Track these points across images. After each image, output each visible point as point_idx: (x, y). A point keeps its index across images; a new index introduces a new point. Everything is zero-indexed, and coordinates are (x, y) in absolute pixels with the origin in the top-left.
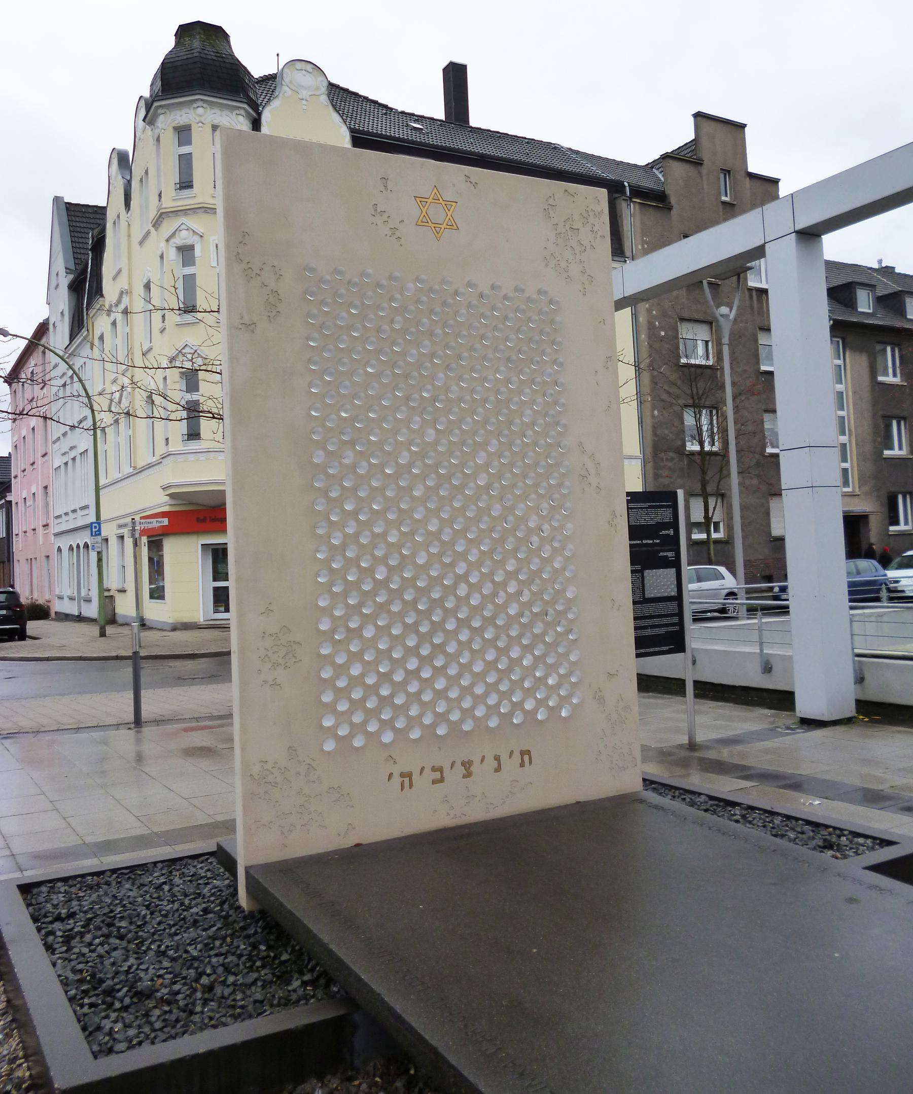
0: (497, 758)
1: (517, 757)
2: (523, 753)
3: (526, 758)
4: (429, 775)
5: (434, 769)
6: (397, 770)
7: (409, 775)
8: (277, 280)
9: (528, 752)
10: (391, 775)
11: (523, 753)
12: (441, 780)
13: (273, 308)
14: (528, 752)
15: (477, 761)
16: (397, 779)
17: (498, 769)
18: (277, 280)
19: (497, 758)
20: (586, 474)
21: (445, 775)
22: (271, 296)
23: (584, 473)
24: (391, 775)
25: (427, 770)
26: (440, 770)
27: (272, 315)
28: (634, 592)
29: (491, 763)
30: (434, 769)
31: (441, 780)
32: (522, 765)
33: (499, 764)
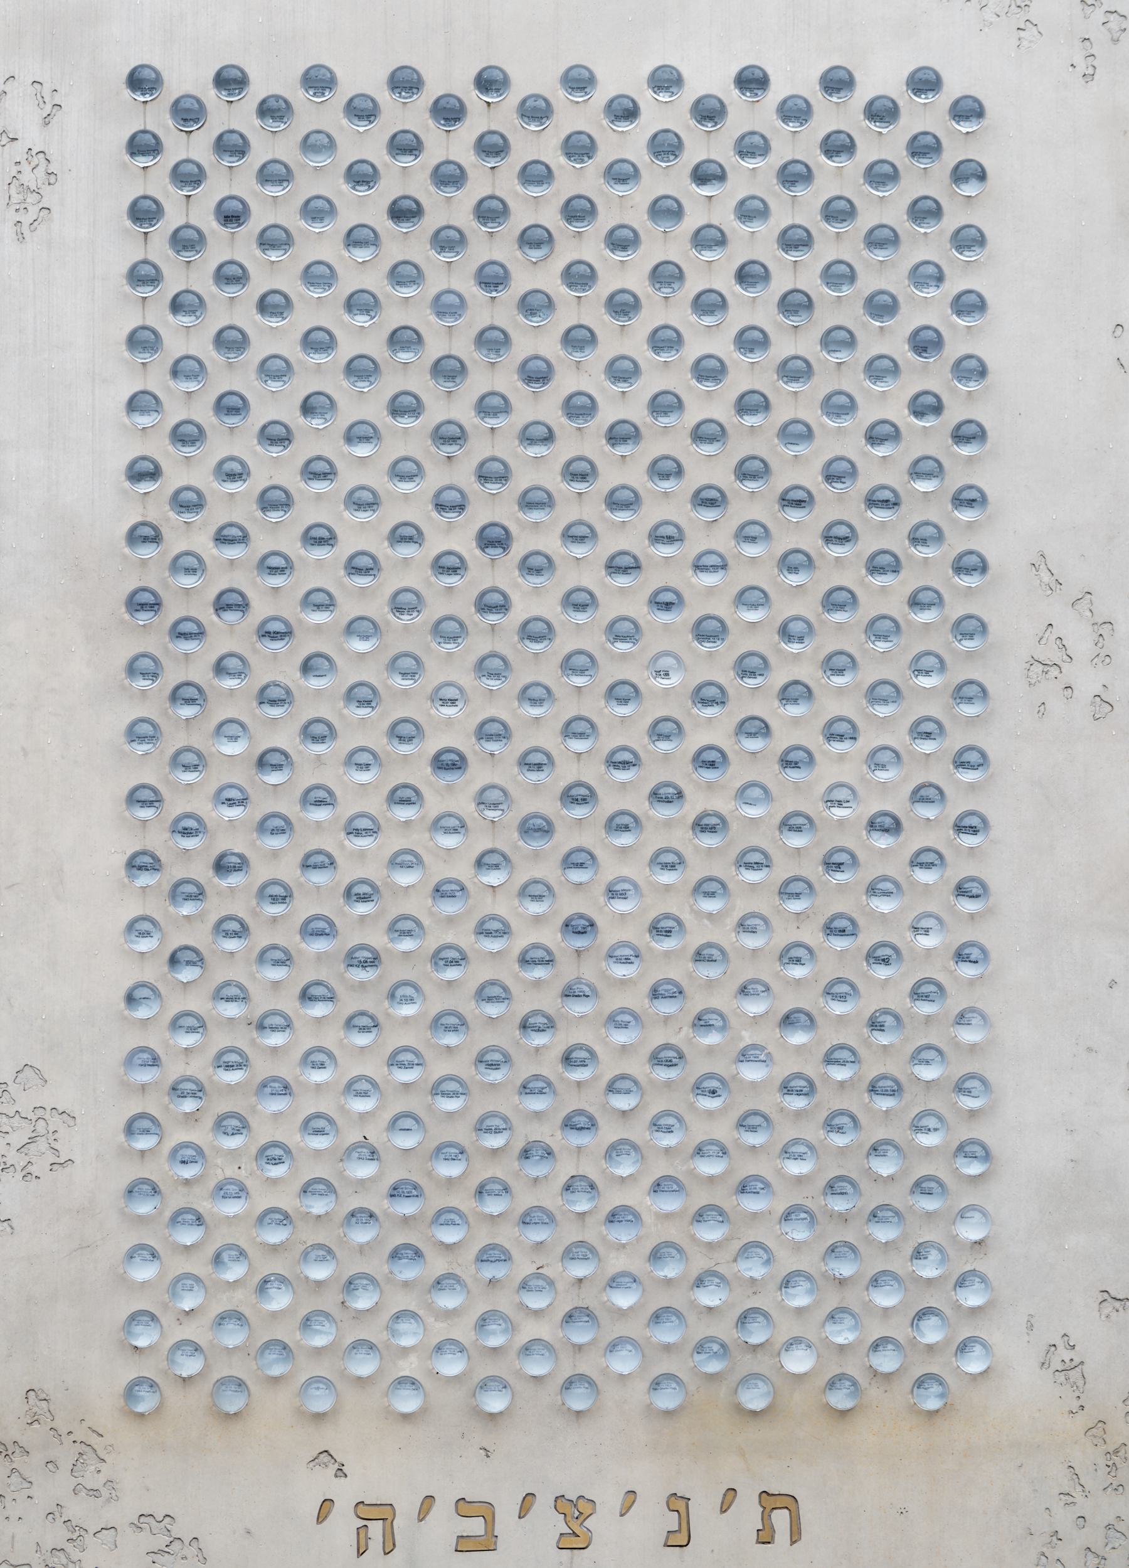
0: (678, 1503)
1: (748, 1512)
2: (769, 1500)
3: (781, 1519)
4: (445, 1525)
5: (464, 1508)
6: (346, 1494)
7: (385, 1513)
8: (47, 121)
9: (790, 1503)
10: (327, 1505)
11: (769, 1500)
12: (487, 1543)
13: (32, 198)
14: (790, 1503)
15: (608, 1499)
16: (343, 1524)
17: (679, 1539)
18: (47, 121)
19: (678, 1503)
20: (1056, 656)
21: (236, 851)
22: (26, 168)
23: (1051, 653)
24: (327, 1505)
25: (443, 1510)
26: (487, 1512)
27: (27, 219)
28: (532, 1505)
29: (654, 1521)
30: (464, 1508)
31: (487, 1543)
32: (765, 1537)
33: (685, 1519)
